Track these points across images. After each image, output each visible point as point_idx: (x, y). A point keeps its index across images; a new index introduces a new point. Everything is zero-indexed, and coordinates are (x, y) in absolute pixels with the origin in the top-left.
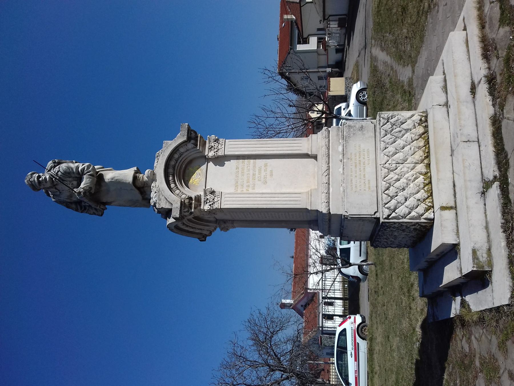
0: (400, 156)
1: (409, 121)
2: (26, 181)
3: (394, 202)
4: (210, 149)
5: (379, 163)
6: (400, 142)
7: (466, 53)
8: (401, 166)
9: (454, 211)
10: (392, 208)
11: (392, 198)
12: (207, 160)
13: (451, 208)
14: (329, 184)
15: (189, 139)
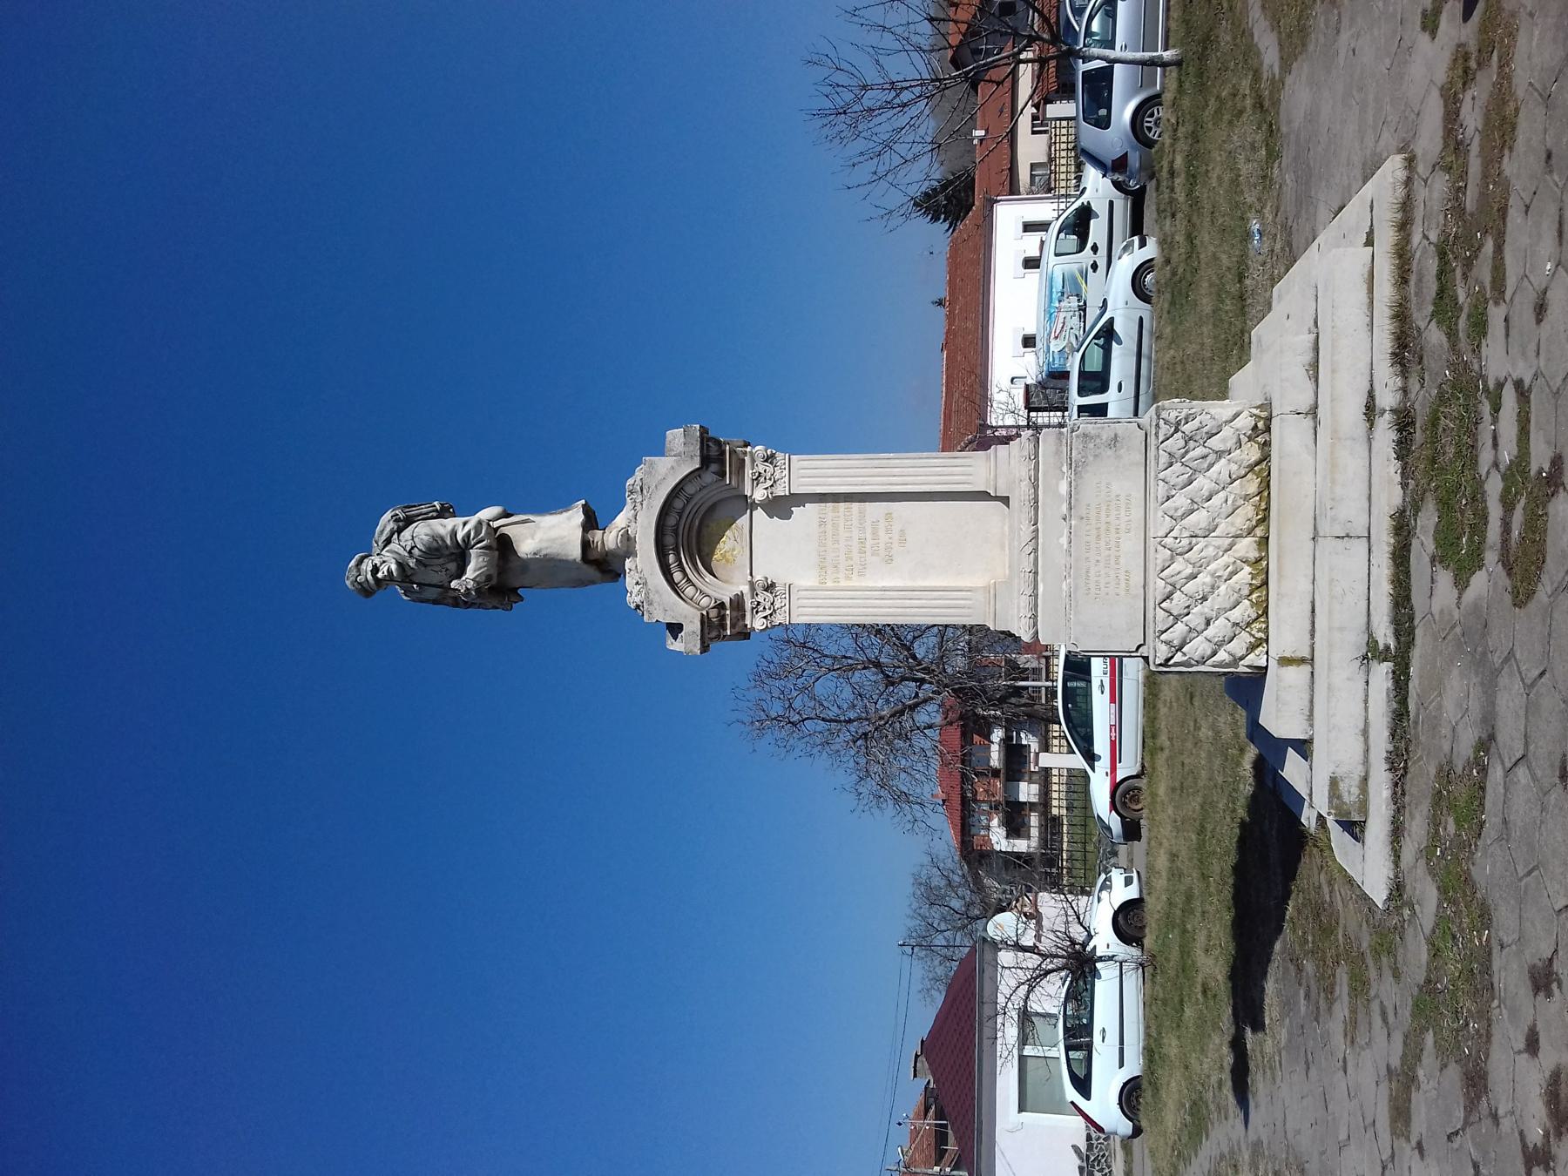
0: (1199, 519)
1: (1227, 431)
2: (348, 583)
3: (1180, 628)
4: (757, 479)
5: (1151, 534)
6: (1203, 483)
7: (1365, 308)
8: (1203, 542)
9: (1309, 668)
10: (1176, 643)
11: (1177, 619)
12: (749, 505)
13: (1302, 661)
14: (1036, 573)
15: (706, 461)
